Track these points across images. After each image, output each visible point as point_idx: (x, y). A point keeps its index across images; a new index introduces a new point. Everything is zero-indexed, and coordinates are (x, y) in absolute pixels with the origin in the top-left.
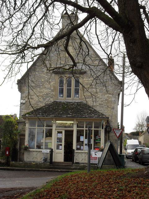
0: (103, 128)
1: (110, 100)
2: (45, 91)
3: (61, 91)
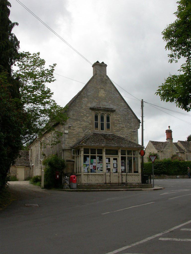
1: (133, 133)
2: (85, 124)
3: (97, 126)
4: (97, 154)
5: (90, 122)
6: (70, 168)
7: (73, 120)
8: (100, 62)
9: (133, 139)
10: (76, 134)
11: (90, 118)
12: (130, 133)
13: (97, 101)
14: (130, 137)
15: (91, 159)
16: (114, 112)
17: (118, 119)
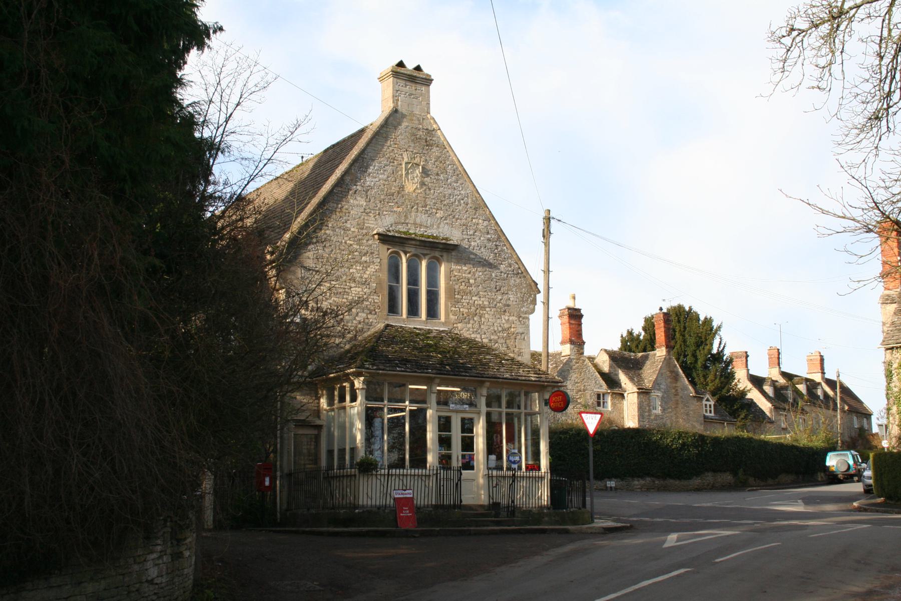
6: (305, 451)
8: (410, 65)
16: (453, 250)
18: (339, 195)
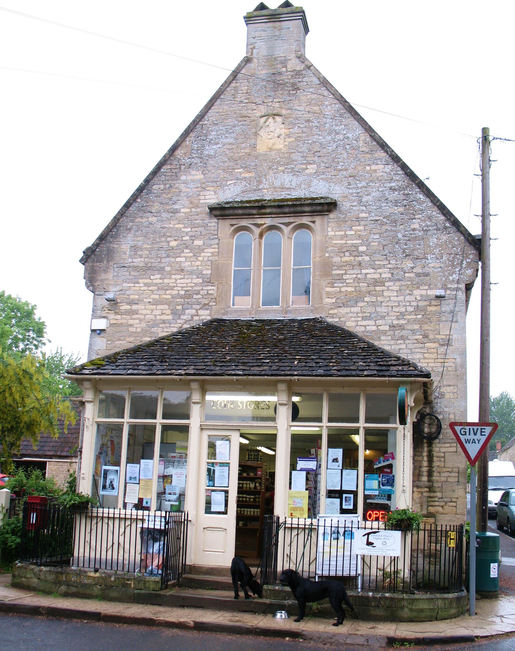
0: (403, 421)
4: (367, 421)
5: (209, 272)
7: (133, 273)
9: (431, 337)
10: (139, 330)
11: (208, 253)
12: (417, 308)
13: (247, 175)
14: (416, 327)
15: (329, 449)
16: (330, 211)
17: (353, 245)
18: (167, 174)
